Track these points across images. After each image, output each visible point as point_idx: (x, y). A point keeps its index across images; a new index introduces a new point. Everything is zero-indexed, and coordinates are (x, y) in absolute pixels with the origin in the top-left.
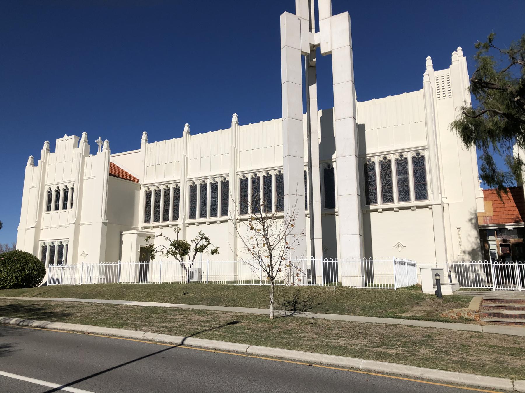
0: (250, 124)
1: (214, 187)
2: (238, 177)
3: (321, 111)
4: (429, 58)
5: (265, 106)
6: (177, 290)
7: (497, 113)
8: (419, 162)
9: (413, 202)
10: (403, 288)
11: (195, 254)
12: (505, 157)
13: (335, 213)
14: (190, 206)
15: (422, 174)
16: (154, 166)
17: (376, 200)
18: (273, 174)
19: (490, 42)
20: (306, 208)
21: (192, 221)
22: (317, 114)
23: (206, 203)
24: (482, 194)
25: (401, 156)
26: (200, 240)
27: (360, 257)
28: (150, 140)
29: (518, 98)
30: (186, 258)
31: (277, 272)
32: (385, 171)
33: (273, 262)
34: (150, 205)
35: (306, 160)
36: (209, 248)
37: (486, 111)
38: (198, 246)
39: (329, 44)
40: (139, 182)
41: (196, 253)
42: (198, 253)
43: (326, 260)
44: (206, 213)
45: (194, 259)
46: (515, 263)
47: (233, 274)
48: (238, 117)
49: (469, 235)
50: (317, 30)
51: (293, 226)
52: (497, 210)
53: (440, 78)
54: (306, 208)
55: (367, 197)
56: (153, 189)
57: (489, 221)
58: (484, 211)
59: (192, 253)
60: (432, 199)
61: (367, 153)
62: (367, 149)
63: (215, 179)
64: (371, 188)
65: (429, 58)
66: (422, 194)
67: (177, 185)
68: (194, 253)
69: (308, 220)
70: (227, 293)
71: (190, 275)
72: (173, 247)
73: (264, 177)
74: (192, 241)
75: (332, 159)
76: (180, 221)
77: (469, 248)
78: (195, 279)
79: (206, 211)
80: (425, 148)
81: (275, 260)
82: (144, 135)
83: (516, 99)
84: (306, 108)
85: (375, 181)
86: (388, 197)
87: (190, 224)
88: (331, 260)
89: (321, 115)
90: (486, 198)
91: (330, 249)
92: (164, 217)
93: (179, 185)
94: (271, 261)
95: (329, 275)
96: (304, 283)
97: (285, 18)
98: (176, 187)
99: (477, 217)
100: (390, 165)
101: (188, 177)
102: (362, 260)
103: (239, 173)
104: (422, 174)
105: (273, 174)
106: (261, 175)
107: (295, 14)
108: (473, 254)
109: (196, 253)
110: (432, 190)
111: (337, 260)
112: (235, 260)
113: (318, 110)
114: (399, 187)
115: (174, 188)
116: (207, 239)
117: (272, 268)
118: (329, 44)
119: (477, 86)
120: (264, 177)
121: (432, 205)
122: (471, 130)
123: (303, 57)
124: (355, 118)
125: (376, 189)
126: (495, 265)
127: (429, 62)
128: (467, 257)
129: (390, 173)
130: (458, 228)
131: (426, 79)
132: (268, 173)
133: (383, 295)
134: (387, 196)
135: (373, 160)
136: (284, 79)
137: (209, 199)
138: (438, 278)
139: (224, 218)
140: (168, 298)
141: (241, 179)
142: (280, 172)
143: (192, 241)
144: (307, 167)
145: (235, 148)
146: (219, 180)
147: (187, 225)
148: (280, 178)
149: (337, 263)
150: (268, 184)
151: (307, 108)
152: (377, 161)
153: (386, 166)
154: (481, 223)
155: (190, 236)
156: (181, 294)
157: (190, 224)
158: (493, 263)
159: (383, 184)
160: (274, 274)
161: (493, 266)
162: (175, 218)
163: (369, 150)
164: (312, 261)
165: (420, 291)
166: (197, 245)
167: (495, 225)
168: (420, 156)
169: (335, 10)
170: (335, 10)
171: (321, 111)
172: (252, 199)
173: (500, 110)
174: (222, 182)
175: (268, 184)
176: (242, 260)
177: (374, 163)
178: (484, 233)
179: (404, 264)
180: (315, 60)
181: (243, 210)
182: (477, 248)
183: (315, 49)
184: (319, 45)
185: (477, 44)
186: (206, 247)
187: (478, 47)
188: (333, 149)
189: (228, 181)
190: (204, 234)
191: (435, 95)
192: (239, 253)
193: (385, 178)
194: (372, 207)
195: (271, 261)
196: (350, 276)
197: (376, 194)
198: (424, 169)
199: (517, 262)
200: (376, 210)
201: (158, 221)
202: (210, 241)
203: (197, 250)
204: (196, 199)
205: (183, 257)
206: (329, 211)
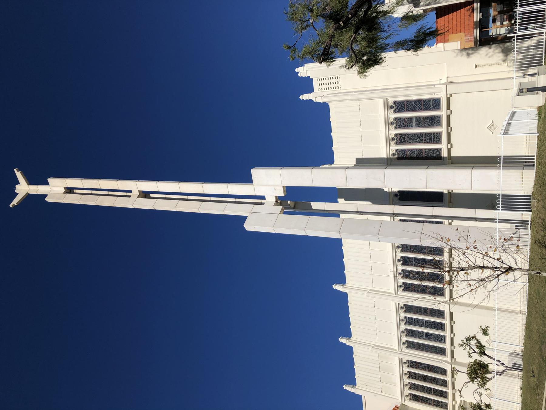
0: (345, 272)
1: (410, 321)
2: (401, 293)
3: (338, 200)
4: (301, 97)
5: (328, 255)
6: (529, 385)
7: (355, 38)
8: (399, 106)
9: (442, 113)
10: (538, 126)
11: (487, 355)
12: (400, 28)
13: (449, 193)
14: (431, 352)
15: (413, 103)
16: (382, 384)
17: (437, 149)
18: (400, 255)
19: (290, 47)
20: (441, 223)
21: (448, 352)
22: (342, 204)
23: (429, 333)
24: (440, 45)
25: (392, 123)
26: (470, 347)
27: (498, 170)
28: (353, 383)
29: (341, 22)
30: (492, 367)
31: (502, 262)
32: (407, 139)
33: (490, 265)
34: (427, 398)
35: (387, 218)
36: (483, 340)
37: (352, 48)
38: (477, 350)
39: (276, 188)
40: (399, 405)
41: (485, 354)
42: (486, 352)
43: (499, 207)
44: (440, 335)
45: (491, 358)
46: (516, 12)
47: (519, 315)
48: (337, 283)
49: (487, 55)
50: (263, 198)
51: (448, 240)
52: (459, 29)
53: (321, 87)
54: (441, 223)
55: (433, 159)
56: (408, 391)
57: (470, 36)
58: (459, 42)
59: (485, 360)
60: (441, 94)
61: (386, 157)
62: (382, 156)
63: (401, 318)
64: (424, 155)
65: (301, 97)
66: (435, 104)
67: (405, 363)
68: (485, 356)
69: (456, 223)
70: (535, 325)
71: (515, 367)
72: (476, 380)
73: (402, 264)
74: (470, 356)
75: (389, 192)
76: (448, 368)
77: (501, 56)
78: (520, 361)
79: (437, 335)
80: (386, 101)
81: (487, 264)
82: (347, 388)
83: (342, 25)
84: (335, 214)
85: (417, 150)
86: (435, 138)
87: (452, 356)
88: (499, 201)
89: (343, 200)
90: (445, 41)
91: (488, 201)
92: (442, 385)
93: (404, 361)
94: (488, 268)
95: (524, 205)
96: (528, 232)
97: (249, 226)
98: (407, 364)
99: (465, 49)
100: (401, 135)
101: (397, 348)
102: (500, 169)
103: (397, 292)
104: (413, 103)
105: (400, 255)
106: (400, 268)
107: (247, 217)
108: (507, 52)
109: (485, 354)
110: (430, 94)
111: (499, 195)
112: (495, 310)
113: (338, 202)
114: (425, 126)
115: (408, 366)
116: (469, 339)
117: (496, 268)
118: (276, 188)
119: (326, 56)
120: (402, 264)
121: (447, 94)
122: (368, 60)
123: (285, 213)
124: (347, 168)
125: (425, 149)
126: (517, 31)
127: (305, 97)
128: (510, 57)
129: (409, 134)
130: (476, 67)
131: (319, 100)
132: (399, 260)
133: (543, 148)
134: (434, 139)
135: (393, 151)
136: (302, 233)
137: (424, 329)
138: (525, 90)
139: (447, 315)
140: (538, 397)
141: (404, 290)
142: (398, 247)
143: (470, 356)
144: (395, 218)
145: (368, 292)
146: (403, 315)
147: (453, 360)
148: (405, 248)
149: (503, 195)
150: (410, 262)
151: (335, 212)
152: (395, 147)
153: (401, 139)
154: (472, 44)
155: (464, 357)
156: (533, 380)
157: (452, 356)
158: (515, 33)
159: (420, 142)
160: (505, 266)
161: (519, 33)
162: (444, 372)
163: (383, 154)
164: (499, 222)
165: (543, 107)
166: (475, 352)
167: (475, 31)
168: (394, 106)
169: (248, 180)
170: (248, 180)
171: (338, 200)
172: (415, 279)
173: (352, 36)
174: (405, 311)
175: (410, 262)
176: (484, 299)
177: (397, 150)
178: (485, 41)
179: (509, 124)
180: (289, 202)
181: (439, 292)
182: (501, 48)
183: (280, 201)
184: (276, 197)
185: (291, 59)
186: (478, 342)
187: (294, 58)
188: (379, 191)
189: (405, 305)
190: (462, 341)
191: (336, 91)
192: (476, 303)
193: (414, 139)
194: (445, 154)
195: (488, 268)
196: (523, 182)
197: (430, 150)
198: (408, 102)
199: (516, 10)
200: (449, 151)
201: (446, 393)
202: (472, 335)
203: (482, 353)
204: (423, 344)
205: (489, 370)
206: (446, 199)
